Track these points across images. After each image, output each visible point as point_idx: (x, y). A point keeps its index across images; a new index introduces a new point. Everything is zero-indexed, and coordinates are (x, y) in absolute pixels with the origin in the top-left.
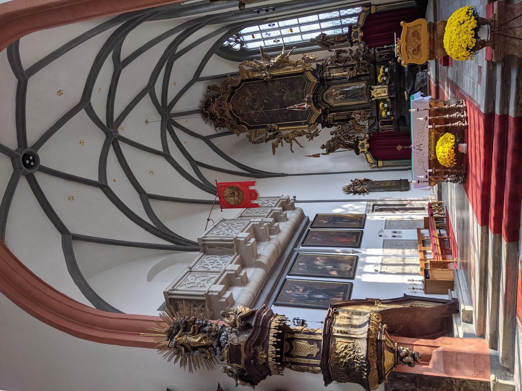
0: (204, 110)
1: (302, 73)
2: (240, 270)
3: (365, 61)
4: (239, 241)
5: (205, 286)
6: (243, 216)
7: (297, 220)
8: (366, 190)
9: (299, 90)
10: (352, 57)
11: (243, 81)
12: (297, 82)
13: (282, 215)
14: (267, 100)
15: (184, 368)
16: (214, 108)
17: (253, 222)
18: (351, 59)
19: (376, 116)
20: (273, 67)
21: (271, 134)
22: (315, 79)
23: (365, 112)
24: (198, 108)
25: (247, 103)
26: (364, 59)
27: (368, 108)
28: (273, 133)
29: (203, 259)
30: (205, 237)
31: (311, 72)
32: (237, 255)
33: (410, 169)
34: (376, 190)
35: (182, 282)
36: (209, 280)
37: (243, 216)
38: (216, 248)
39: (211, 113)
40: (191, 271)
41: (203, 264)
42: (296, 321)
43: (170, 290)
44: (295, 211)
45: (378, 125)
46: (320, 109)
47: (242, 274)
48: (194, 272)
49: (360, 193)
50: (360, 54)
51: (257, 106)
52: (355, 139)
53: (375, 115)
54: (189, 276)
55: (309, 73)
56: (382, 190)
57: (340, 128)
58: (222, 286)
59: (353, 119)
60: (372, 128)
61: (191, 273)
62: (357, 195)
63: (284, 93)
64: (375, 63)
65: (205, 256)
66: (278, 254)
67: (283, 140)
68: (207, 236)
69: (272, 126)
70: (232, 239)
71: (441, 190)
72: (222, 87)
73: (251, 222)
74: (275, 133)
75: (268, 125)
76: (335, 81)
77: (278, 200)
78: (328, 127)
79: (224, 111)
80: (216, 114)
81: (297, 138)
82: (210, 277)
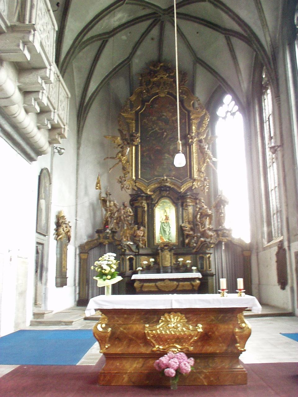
0: (162, 64)
1: (191, 177)
3: (199, 243)
4: (30, 32)
8: (60, 237)
9: (174, 173)
10: (205, 231)
14: (167, 136)
16: (163, 76)
18: (203, 229)
20: (200, 146)
22: (184, 190)
23: (144, 242)
24: (164, 58)
25: (165, 114)
26: (202, 242)
27: (149, 246)
31: (191, 187)
32: (7, 27)
39: (155, 72)
46: (152, 193)
49: (57, 230)
50: (207, 238)
51: (161, 124)
53: (141, 252)
55: (191, 184)
56: (58, 256)
57: (131, 213)
60: (128, 248)
62: (55, 227)
67: (119, 149)
69: (138, 138)
70: (33, 22)
71: (63, 325)
72: (184, 88)
75: (139, 135)
76: (181, 211)
78: (130, 201)
79: (158, 86)
81: (120, 166)
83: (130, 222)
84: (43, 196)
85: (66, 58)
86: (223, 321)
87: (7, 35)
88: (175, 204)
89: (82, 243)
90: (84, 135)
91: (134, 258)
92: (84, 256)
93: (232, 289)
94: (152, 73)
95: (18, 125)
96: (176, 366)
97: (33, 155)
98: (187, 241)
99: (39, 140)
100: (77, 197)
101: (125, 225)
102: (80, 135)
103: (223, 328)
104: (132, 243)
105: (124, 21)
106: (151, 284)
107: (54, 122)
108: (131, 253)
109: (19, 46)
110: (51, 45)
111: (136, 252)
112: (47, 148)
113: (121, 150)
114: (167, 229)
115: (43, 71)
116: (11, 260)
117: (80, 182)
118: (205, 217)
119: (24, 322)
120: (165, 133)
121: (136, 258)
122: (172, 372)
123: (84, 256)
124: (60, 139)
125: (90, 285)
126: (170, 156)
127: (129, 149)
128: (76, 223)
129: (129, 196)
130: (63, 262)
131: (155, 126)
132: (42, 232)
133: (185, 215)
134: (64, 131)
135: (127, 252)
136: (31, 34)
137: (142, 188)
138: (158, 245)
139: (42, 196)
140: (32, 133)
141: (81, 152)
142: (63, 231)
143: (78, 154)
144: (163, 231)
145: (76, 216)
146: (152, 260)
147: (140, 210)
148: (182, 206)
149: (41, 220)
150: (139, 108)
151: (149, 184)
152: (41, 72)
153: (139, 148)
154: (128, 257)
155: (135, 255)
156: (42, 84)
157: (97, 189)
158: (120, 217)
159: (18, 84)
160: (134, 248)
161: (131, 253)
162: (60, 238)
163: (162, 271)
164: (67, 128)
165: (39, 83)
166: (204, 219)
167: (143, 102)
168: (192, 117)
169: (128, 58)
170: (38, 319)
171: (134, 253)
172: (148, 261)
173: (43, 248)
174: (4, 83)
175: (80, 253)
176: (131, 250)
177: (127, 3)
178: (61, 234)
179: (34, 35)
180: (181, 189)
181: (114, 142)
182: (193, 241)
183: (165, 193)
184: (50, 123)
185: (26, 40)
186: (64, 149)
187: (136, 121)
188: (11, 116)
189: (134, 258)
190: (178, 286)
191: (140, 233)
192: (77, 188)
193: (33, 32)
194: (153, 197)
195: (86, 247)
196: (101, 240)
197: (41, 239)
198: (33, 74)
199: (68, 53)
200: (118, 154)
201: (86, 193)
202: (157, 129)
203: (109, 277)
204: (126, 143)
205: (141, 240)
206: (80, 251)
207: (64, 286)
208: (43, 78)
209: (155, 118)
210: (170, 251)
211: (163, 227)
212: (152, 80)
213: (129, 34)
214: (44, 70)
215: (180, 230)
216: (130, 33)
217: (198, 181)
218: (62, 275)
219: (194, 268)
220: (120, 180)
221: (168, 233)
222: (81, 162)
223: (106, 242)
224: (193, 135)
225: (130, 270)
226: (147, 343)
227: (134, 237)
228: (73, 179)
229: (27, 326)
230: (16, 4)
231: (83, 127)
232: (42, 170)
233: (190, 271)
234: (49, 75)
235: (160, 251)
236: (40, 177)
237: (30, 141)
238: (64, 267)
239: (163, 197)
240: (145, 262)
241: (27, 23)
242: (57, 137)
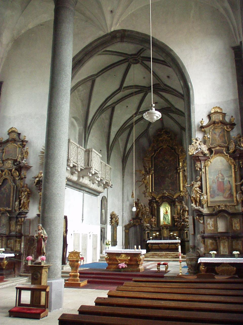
0: (164, 130)
3: (181, 225)
4: (91, 169)
8: (113, 224)
9: (171, 188)
10: (184, 218)
11: (178, 155)
12: (175, 187)
13: (101, 184)
14: (167, 169)
15: (40, 153)
16: (165, 137)
17: (99, 174)
19: (153, 230)
21: (148, 170)
23: (155, 224)
26: (183, 224)
28: (148, 171)
31: (180, 195)
33: (123, 249)
34: (112, 229)
35: (73, 145)
40: (78, 148)
44: (103, 189)
45: (148, 231)
47: (76, 172)
48: (78, 149)
49: (111, 221)
50: (186, 222)
52: (141, 218)
55: (179, 194)
56: (112, 232)
59: (152, 218)
63: (170, 179)
64: (180, 230)
67: (144, 177)
68: (94, 152)
69: (152, 171)
74: (148, 172)
78: (149, 203)
80: (161, 137)
81: (144, 185)
83: (148, 214)
84: (103, 208)
85: (112, 144)
86: (135, 256)
88: (171, 205)
89: (126, 225)
90: (126, 170)
91: (150, 232)
92: (127, 231)
93: (137, 248)
94: (159, 135)
96: (122, 266)
97: (97, 194)
98: (176, 224)
100: (123, 202)
101: (145, 216)
103: (134, 258)
104: (149, 225)
106: (156, 245)
108: (148, 230)
109: (88, 174)
111: (151, 230)
113: (144, 177)
114: (167, 218)
115: (97, 174)
116: (90, 236)
117: (124, 194)
118: (185, 212)
119: (96, 260)
120: (166, 167)
121: (151, 233)
122: (121, 267)
123: (127, 231)
125: (130, 245)
126: (169, 179)
127: (148, 176)
128: (123, 215)
129: (148, 201)
130: (115, 235)
131: (161, 163)
132: (103, 222)
133: (175, 210)
134: (109, 184)
135: (146, 229)
137: (155, 196)
138: (161, 226)
139: (103, 208)
141: (125, 179)
142: (114, 221)
143: (123, 180)
144: (164, 218)
145: (123, 212)
146: (158, 233)
147: (153, 209)
148: (174, 206)
149: (103, 219)
150: (153, 154)
151: (158, 195)
153: (153, 175)
154: (147, 232)
155: (150, 231)
157: (132, 198)
158: (143, 212)
159: (89, 179)
160: (150, 227)
161: (148, 230)
162: (113, 225)
163: (162, 239)
166: (184, 213)
167: (155, 151)
168: (180, 158)
169: (146, 130)
170: (102, 259)
171: (150, 230)
172: (156, 234)
173: (104, 229)
175: (125, 229)
176: (148, 228)
178: (113, 222)
180: (174, 197)
181: (141, 173)
182: (179, 224)
183: (165, 200)
187: (151, 161)
189: (150, 232)
190: (169, 246)
191: (153, 220)
192: (123, 198)
193: (92, 169)
194: (159, 201)
195: (128, 227)
196: (135, 223)
197: (103, 226)
199: (113, 141)
200: (142, 179)
201: (128, 200)
202: (162, 165)
203: (108, 245)
204: (146, 173)
205: (153, 223)
206: (125, 228)
207: (116, 246)
209: (161, 160)
210: (167, 229)
211: (165, 217)
212: (159, 139)
215: (173, 218)
217: (183, 192)
218: (114, 241)
219: (177, 238)
220: (144, 192)
221: (167, 220)
222: (125, 184)
223: (137, 224)
224: (180, 168)
225: (148, 238)
226: (117, 261)
227: (150, 222)
228: (121, 193)
229: (98, 261)
231: (125, 167)
232: (103, 197)
233: (176, 239)
235: (162, 229)
236: (101, 201)
238: (115, 237)
239: (164, 201)
240: (154, 235)
241: (90, 166)
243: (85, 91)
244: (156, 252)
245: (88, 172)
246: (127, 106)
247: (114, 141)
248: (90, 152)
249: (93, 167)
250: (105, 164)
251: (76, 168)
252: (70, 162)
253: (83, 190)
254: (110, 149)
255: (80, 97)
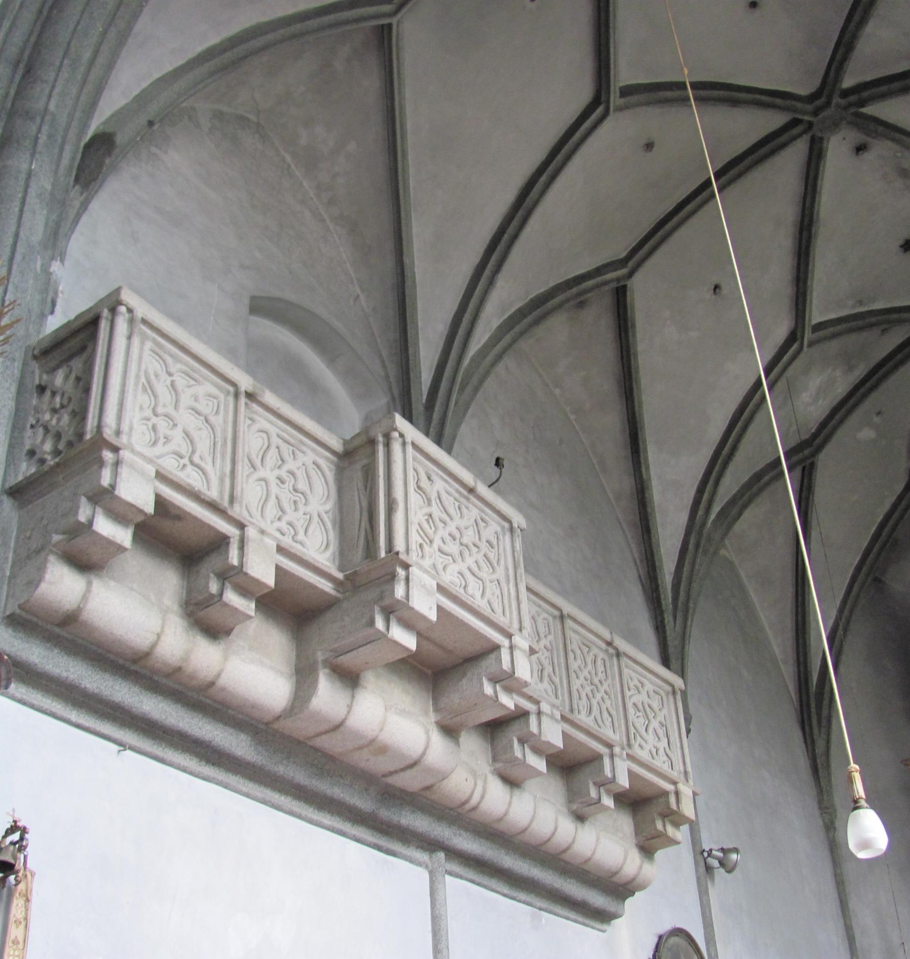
2: (246, 588)
4: (393, 577)
5: (155, 443)
6: (562, 623)
7: (106, 671)
29: (314, 450)
30: (404, 444)
36: (192, 463)
37: (562, 623)
38: (362, 497)
41: (284, 447)
42: (16, 837)
43: (130, 311)
54: (215, 391)
58: (270, 580)
61: (231, 399)
65: (327, 459)
66: (396, 772)
73: (509, 636)
77: (674, 774)
82: (209, 468)
87: (345, 605)
95: (501, 827)
97: (597, 899)
99: (593, 854)
102: (823, 782)
105: (841, 389)
107: (620, 785)
109: (372, 622)
110: (507, 576)
112: (641, 867)
124: (670, 830)
136: (399, 581)
140: (554, 840)
152: (489, 663)
156: (497, 697)
164: (686, 790)
165: (486, 696)
174: (381, 730)
177: (810, 345)
179: (407, 579)
184: (608, 792)
185: (387, 602)
186: (736, 850)
188: (459, 810)
193: (401, 572)
198: (469, 675)
208: (495, 680)
213: (877, 420)
214: (493, 656)
216: (879, 413)
230: (357, 514)
234: (509, 665)
237: (567, 863)
241: (383, 554)
242: (659, 825)
243: (352, 147)
244: (299, 580)
245: (377, 609)
246: (716, 287)
247: (691, 547)
248: (381, 449)
249: (413, 558)
250: (609, 644)
251: (227, 551)
252: (117, 464)
253: (431, 845)
254: (675, 608)
255: (331, 202)
